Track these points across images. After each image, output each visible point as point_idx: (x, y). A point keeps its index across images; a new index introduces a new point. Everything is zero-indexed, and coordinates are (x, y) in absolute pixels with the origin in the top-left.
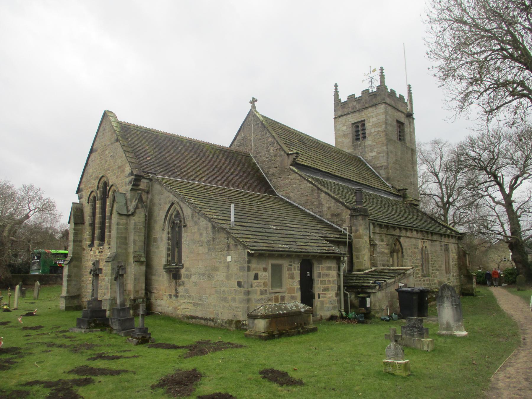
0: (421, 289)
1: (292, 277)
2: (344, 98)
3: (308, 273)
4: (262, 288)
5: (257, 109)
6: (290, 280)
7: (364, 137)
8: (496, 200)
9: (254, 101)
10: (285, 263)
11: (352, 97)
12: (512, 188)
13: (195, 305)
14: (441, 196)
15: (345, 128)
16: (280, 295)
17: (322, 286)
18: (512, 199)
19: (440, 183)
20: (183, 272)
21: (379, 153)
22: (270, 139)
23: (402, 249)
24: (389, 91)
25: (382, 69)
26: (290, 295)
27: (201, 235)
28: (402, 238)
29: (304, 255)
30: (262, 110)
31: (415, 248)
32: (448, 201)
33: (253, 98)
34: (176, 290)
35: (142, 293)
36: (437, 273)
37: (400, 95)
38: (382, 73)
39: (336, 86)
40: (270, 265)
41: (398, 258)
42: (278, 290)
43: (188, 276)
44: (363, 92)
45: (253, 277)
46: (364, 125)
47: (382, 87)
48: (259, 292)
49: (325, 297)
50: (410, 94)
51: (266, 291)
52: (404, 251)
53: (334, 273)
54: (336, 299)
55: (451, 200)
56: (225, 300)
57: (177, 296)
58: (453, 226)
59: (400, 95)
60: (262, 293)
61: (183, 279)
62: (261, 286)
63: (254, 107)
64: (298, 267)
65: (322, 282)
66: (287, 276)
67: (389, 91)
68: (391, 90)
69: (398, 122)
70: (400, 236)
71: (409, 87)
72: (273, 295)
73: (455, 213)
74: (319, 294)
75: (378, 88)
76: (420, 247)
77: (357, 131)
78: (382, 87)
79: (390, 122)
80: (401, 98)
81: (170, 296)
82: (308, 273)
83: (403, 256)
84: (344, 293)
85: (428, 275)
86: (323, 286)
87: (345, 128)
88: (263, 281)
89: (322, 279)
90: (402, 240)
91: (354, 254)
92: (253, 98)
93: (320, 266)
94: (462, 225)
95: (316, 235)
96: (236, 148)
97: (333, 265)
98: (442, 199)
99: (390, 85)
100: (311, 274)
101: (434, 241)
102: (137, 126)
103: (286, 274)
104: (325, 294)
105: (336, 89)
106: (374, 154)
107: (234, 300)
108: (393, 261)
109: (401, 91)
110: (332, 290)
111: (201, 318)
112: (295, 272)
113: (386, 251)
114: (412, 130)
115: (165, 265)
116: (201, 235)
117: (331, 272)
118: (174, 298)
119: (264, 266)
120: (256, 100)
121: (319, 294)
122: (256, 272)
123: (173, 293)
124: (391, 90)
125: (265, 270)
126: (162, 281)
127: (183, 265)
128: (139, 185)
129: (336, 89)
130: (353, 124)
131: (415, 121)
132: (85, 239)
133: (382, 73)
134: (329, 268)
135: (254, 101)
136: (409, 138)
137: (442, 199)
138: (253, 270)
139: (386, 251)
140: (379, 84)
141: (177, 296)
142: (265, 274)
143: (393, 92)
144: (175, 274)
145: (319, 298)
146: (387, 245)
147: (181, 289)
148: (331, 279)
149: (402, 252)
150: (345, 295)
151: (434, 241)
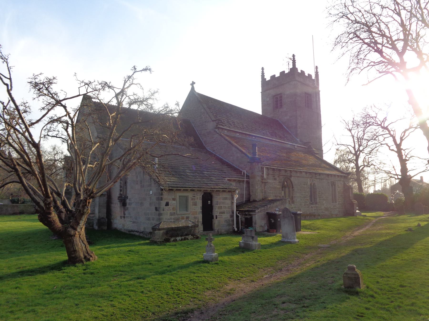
1: (195, 204)
2: (268, 78)
3: (209, 202)
4: (172, 211)
5: (195, 89)
6: (194, 206)
7: (281, 106)
8: (391, 148)
9: (193, 83)
10: (190, 195)
11: (273, 77)
12: (402, 139)
13: (134, 222)
14: (353, 146)
15: (268, 99)
16: (185, 216)
18: (402, 147)
19: (353, 137)
20: (128, 201)
22: (203, 110)
23: (292, 185)
24: (299, 71)
27: (137, 177)
28: (292, 177)
29: (204, 190)
30: (199, 90)
31: (304, 184)
32: (359, 149)
33: (193, 82)
34: (124, 213)
35: (104, 215)
36: (324, 202)
37: (308, 74)
39: (263, 69)
40: (178, 197)
41: (289, 191)
43: (130, 204)
46: (281, 97)
47: (294, 69)
48: (169, 214)
51: (174, 213)
52: (294, 186)
53: (229, 202)
54: (231, 219)
55: (361, 148)
56: (149, 219)
57: (124, 217)
59: (308, 74)
60: (171, 214)
61: (127, 206)
62: (171, 210)
63: (193, 88)
64: (200, 197)
66: (191, 203)
67: (299, 71)
68: (301, 71)
70: (291, 176)
72: (180, 216)
73: (365, 158)
74: (216, 216)
76: (309, 183)
77: (277, 101)
78: (294, 69)
80: (310, 76)
81: (121, 217)
82: (209, 202)
83: (293, 190)
84: (237, 215)
85: (316, 203)
87: (268, 99)
89: (219, 205)
90: (292, 179)
91: (251, 188)
92: (193, 82)
94: (369, 167)
97: (228, 195)
98: (354, 148)
99: (300, 67)
100: (211, 202)
101: (322, 179)
102: (262, 87)
103: (190, 202)
104: (222, 216)
105: (263, 71)
107: (153, 219)
108: (285, 193)
109: (309, 71)
110: (227, 213)
111: (137, 231)
112: (197, 201)
113: (278, 187)
115: (119, 197)
116: (137, 177)
117: (226, 201)
118: (123, 218)
119: (173, 197)
120: (194, 83)
121: (216, 216)
122: (167, 201)
123: (123, 215)
124: (301, 71)
125: (174, 199)
126: (116, 207)
127: (127, 197)
129: (263, 71)
130: (274, 96)
134: (226, 199)
135: (193, 83)
137: (354, 148)
139: (278, 187)
141: (124, 217)
142: (174, 202)
143: (303, 72)
144: (123, 201)
145: (217, 218)
146: (279, 182)
147: (126, 212)
148: (227, 206)
149: (293, 187)
150: (237, 217)
151: (322, 179)
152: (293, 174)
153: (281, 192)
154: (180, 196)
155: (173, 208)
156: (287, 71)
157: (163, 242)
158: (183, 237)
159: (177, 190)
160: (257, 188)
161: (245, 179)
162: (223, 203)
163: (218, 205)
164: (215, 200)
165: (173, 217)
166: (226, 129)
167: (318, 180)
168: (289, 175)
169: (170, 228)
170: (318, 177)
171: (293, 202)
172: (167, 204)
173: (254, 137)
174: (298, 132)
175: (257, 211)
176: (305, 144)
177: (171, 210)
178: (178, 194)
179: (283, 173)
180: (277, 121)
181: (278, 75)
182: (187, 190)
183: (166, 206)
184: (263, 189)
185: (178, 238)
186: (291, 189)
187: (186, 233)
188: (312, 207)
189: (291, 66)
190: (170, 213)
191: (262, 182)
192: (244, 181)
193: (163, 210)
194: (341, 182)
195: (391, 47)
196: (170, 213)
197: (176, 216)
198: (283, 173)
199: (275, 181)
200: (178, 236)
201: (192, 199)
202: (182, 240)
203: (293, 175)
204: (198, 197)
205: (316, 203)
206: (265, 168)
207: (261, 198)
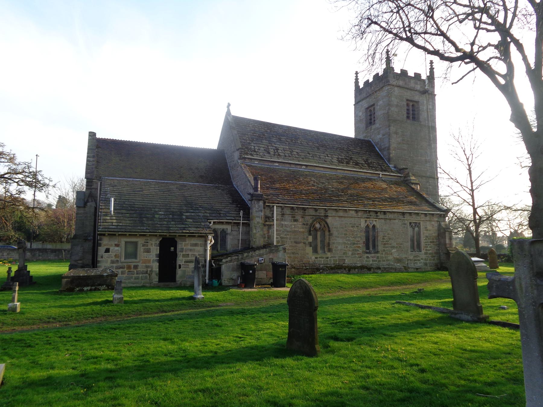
1: (148, 251)
3: (172, 248)
4: (114, 259)
16: (132, 265)
17: (184, 259)
21: (384, 135)
26: (144, 265)
28: (330, 218)
30: (234, 113)
39: (357, 73)
42: (134, 260)
45: (104, 251)
47: (389, 69)
49: (189, 268)
51: (117, 261)
62: (112, 257)
65: (184, 256)
66: (142, 250)
70: (327, 216)
72: (125, 264)
79: (396, 103)
83: (330, 235)
85: (377, 252)
86: (186, 258)
87: (361, 114)
88: (114, 254)
89: (184, 253)
90: (329, 220)
93: (184, 243)
96: (361, 137)
97: (200, 241)
103: (141, 249)
105: (357, 77)
106: (380, 136)
114: (430, 107)
119: (116, 243)
125: (117, 245)
128: (91, 186)
129: (357, 77)
131: (436, 97)
134: (196, 245)
136: (426, 116)
138: (105, 245)
142: (117, 248)
143: (404, 73)
149: (329, 231)
152: (330, 213)
153: (307, 237)
154: (126, 242)
155: (115, 256)
156: (381, 73)
157: (64, 291)
158: (93, 288)
159: (189, 236)
160: (255, 231)
161: (241, 221)
162: (191, 250)
163: (182, 252)
164: (179, 247)
165: (115, 265)
166: (256, 159)
167: (383, 221)
168: (323, 214)
169: (77, 276)
170: (382, 216)
171: (330, 250)
172: (107, 251)
173: (304, 167)
174: (391, 155)
175: (224, 261)
176: (400, 171)
177: (112, 257)
178: (123, 240)
179: (308, 212)
180: (370, 141)
181: (411, 74)
182: (115, 235)
183: (105, 252)
184: (266, 232)
185: (85, 289)
186: (327, 233)
187: (99, 282)
188: (368, 257)
189: (384, 66)
190: (112, 260)
191: (265, 225)
192: (239, 223)
193: (102, 257)
194: (433, 223)
195: (493, 28)
196: (112, 260)
197: (120, 264)
198: (312, 212)
199: (295, 223)
200: (88, 286)
201: (143, 245)
202: (91, 290)
203: (329, 215)
204: (153, 243)
205: (377, 252)
206: (275, 207)
207: (262, 245)
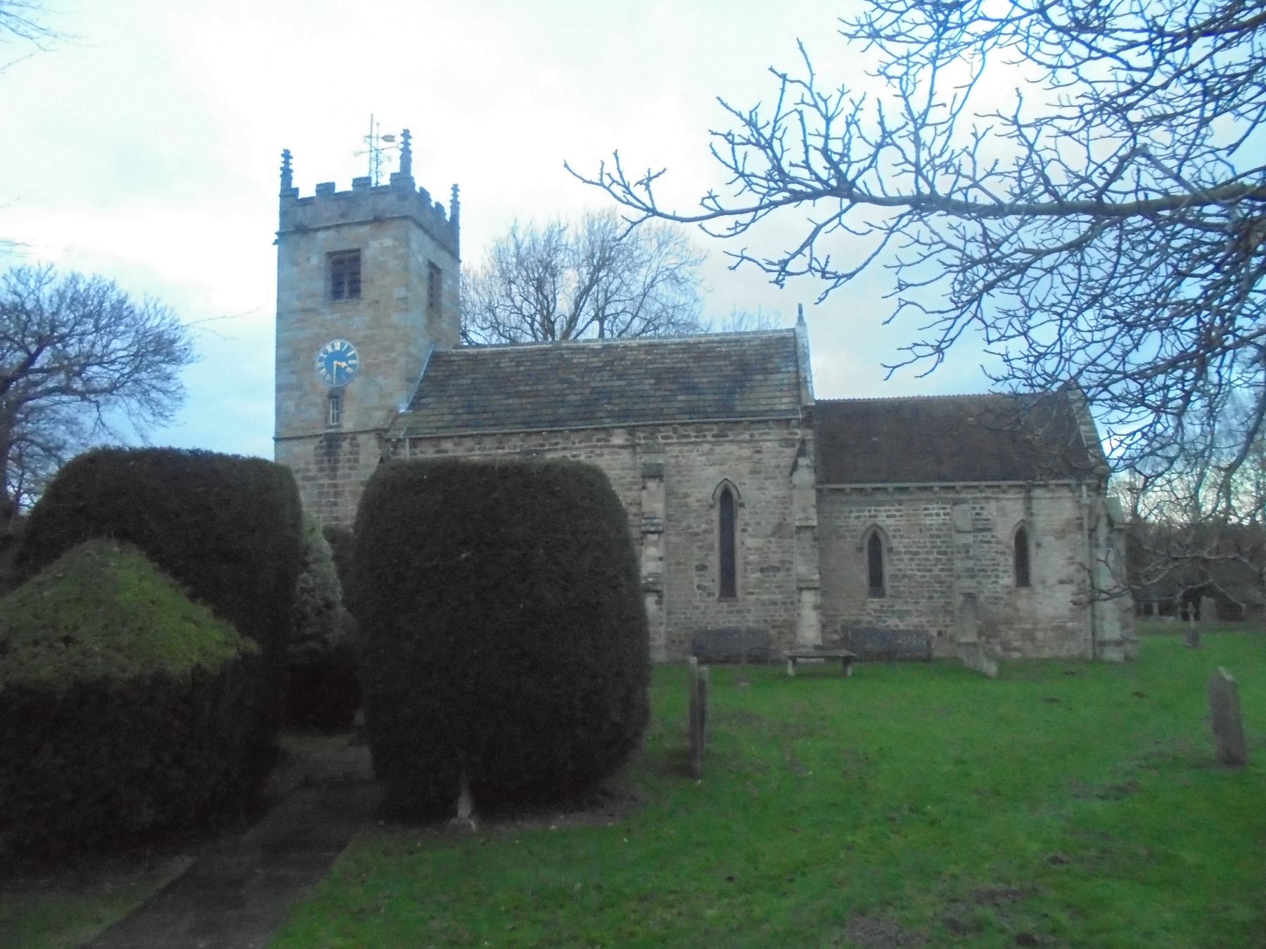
0: (366, 478)
11: (326, 189)
24: (433, 205)
25: (406, 134)
38: (406, 144)
39: (287, 156)
44: (357, 182)
47: (403, 179)
50: (455, 205)
58: (349, 349)
69: (432, 266)
71: (455, 189)
75: (394, 177)
78: (403, 179)
80: (439, 207)
95: (63, 413)
99: (422, 178)
109: (440, 196)
124: (421, 189)
132: (1061, 534)
133: (406, 144)
140: (397, 169)
143: (424, 195)
